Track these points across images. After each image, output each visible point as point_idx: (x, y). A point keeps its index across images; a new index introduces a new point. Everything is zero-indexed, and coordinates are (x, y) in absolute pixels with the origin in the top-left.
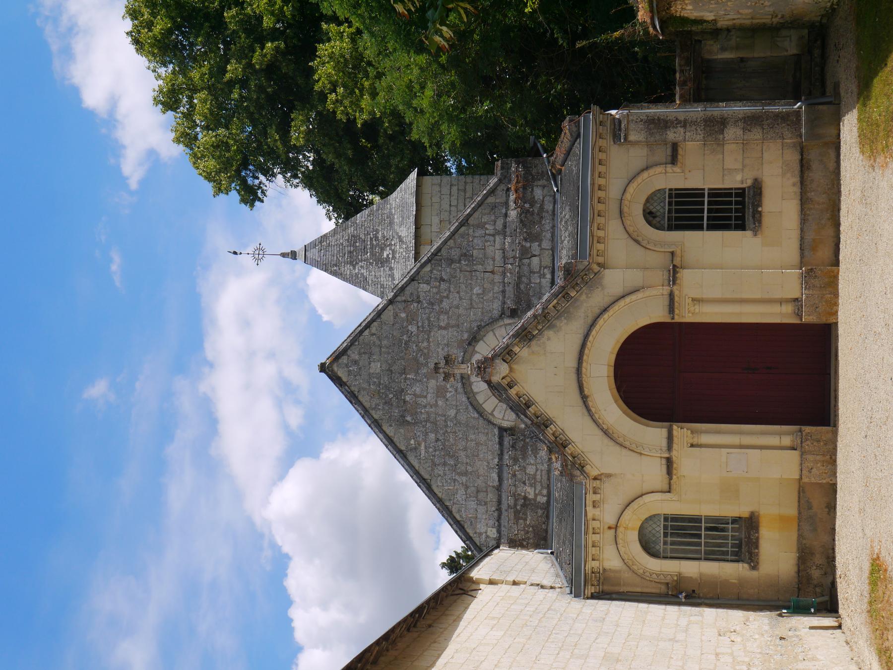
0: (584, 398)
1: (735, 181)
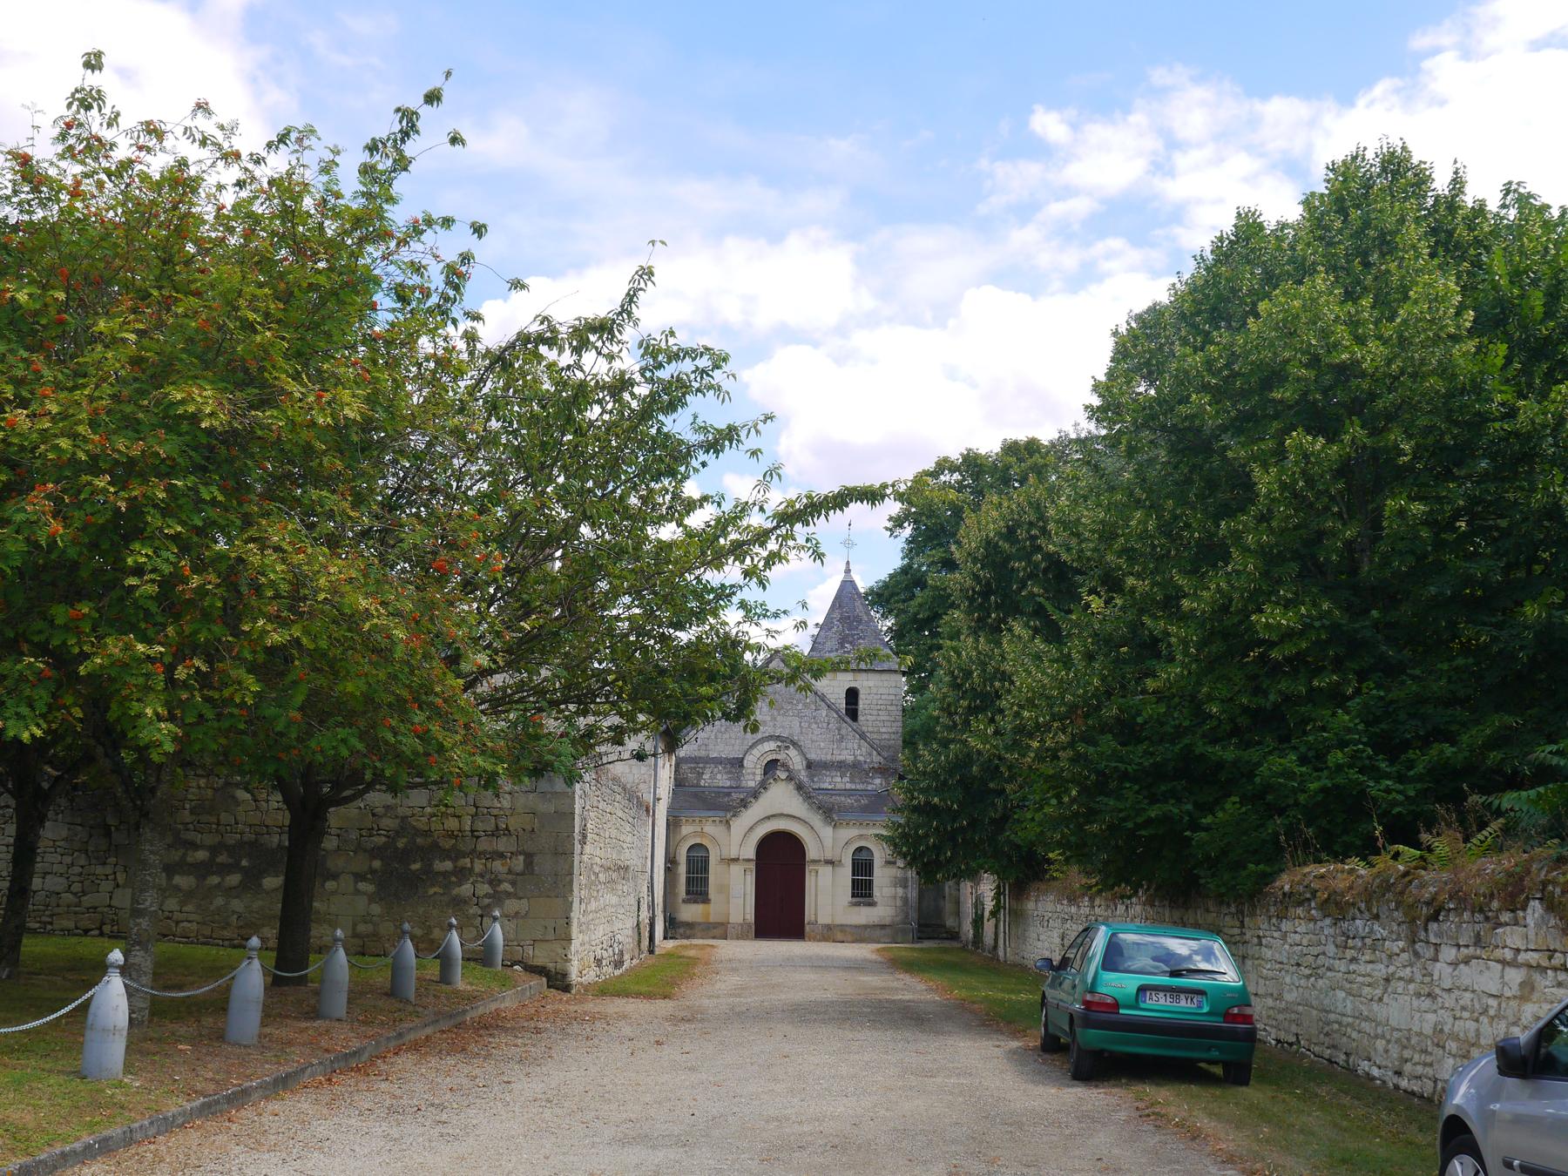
0: (768, 818)
1: (876, 892)
